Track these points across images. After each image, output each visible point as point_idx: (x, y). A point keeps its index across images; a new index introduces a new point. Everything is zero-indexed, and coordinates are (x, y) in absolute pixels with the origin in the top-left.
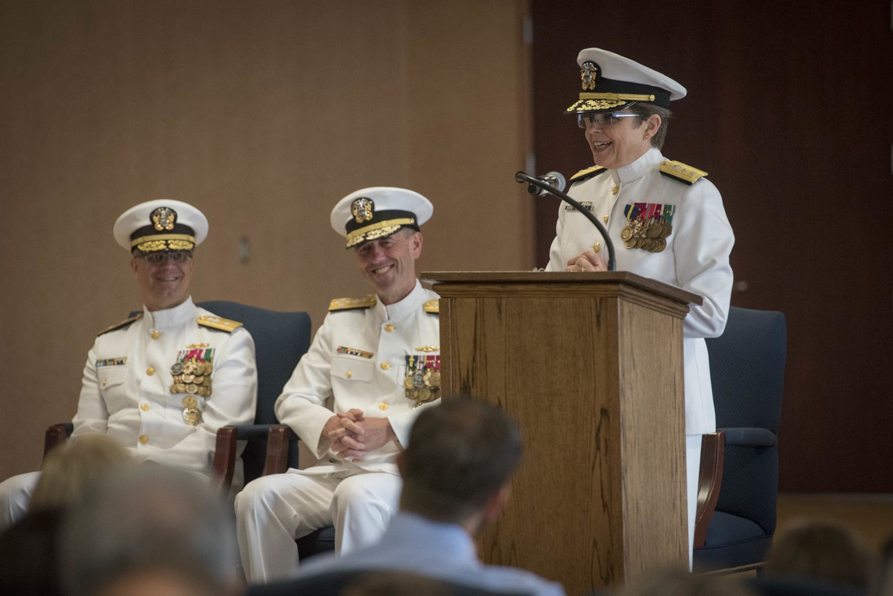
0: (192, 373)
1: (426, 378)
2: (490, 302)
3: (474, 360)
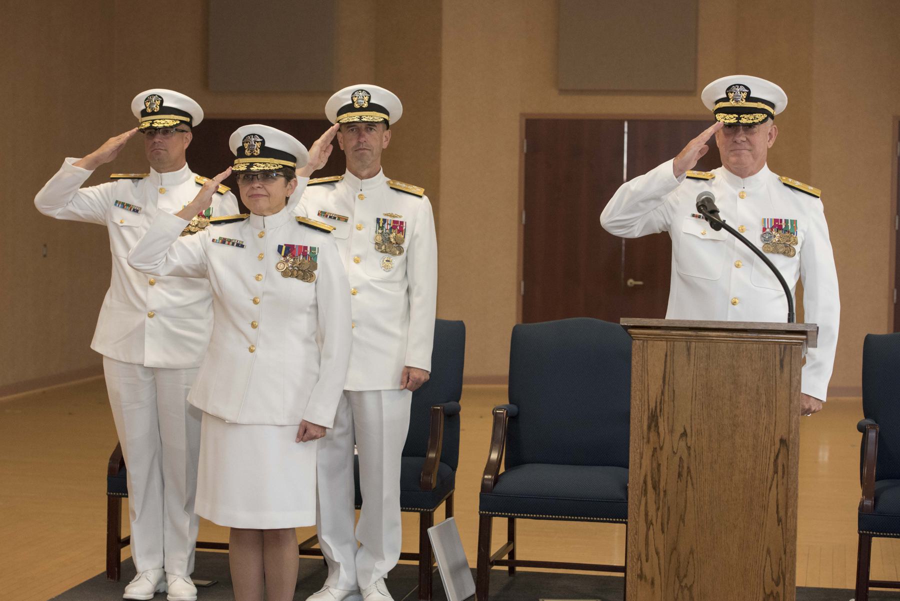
1: (391, 236)
2: (680, 346)
3: (663, 393)
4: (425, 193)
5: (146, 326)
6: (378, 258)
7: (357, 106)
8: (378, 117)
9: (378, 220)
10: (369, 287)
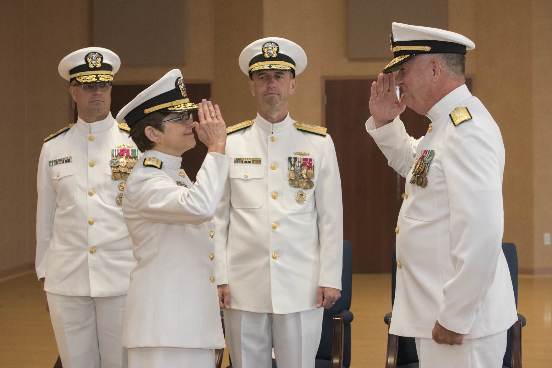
0: (126, 166)
4: (328, 132)
5: (89, 261)
6: (293, 192)
7: (267, 56)
8: (286, 66)
9: (290, 159)
10: (286, 221)
